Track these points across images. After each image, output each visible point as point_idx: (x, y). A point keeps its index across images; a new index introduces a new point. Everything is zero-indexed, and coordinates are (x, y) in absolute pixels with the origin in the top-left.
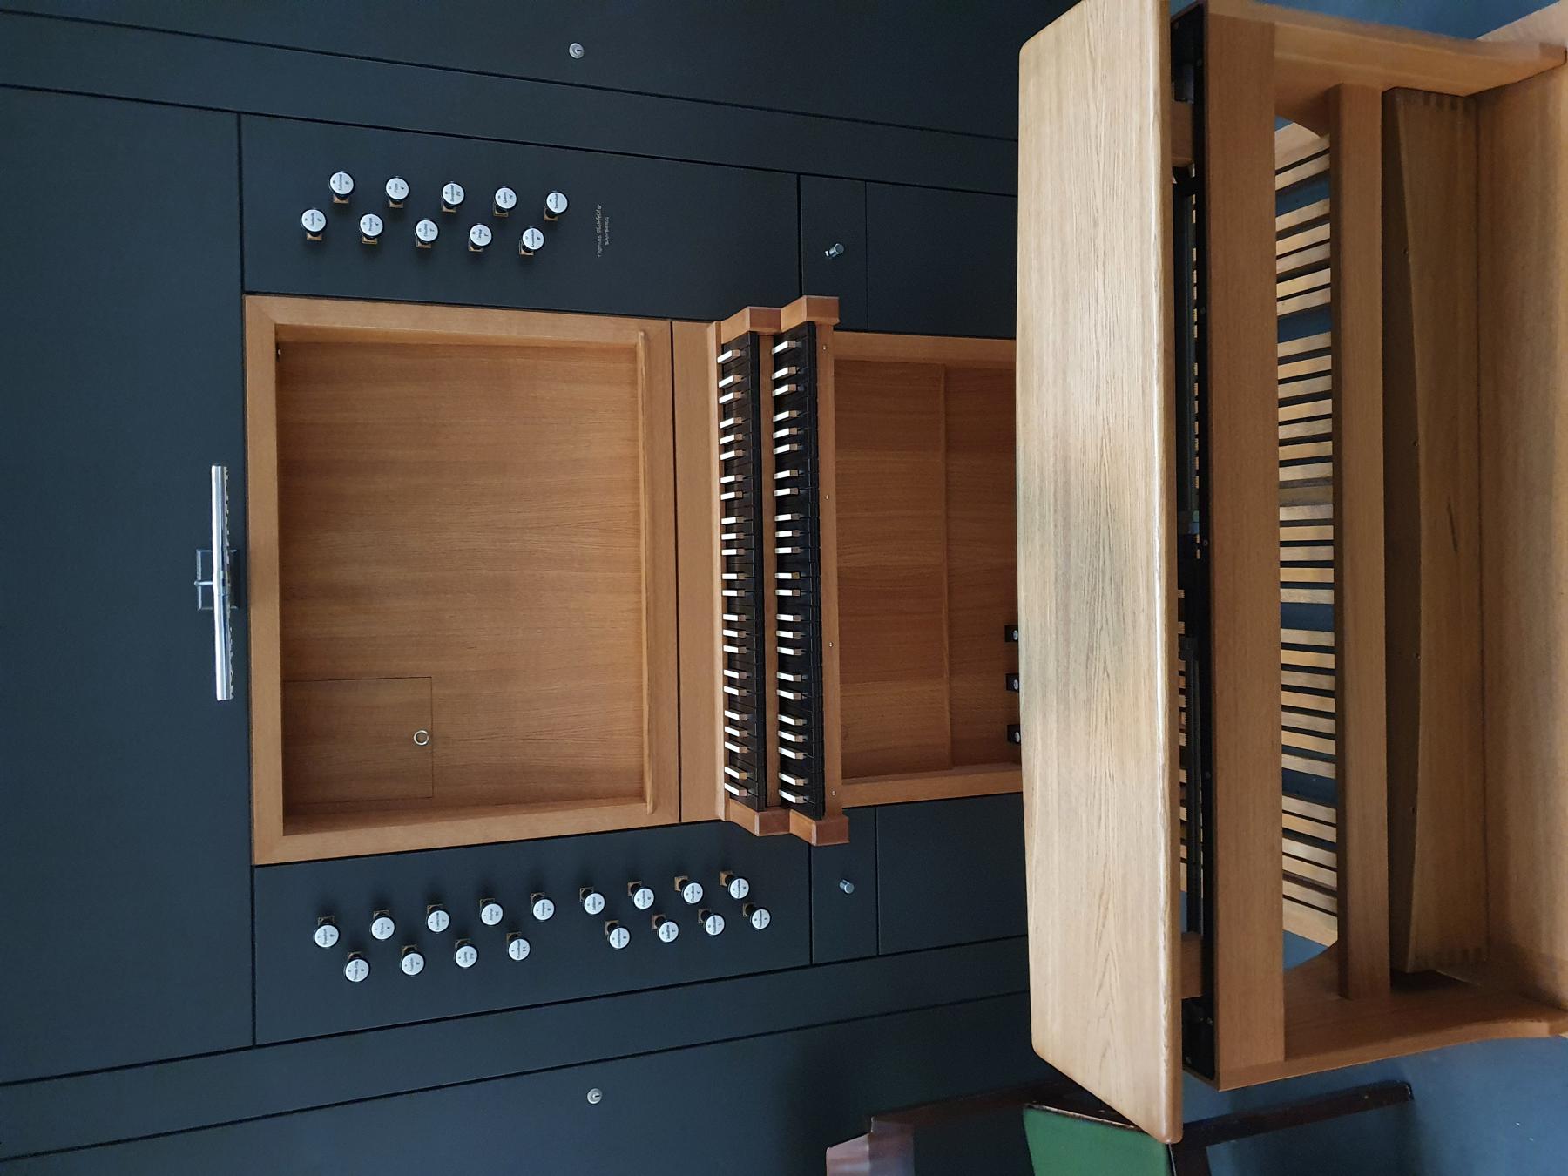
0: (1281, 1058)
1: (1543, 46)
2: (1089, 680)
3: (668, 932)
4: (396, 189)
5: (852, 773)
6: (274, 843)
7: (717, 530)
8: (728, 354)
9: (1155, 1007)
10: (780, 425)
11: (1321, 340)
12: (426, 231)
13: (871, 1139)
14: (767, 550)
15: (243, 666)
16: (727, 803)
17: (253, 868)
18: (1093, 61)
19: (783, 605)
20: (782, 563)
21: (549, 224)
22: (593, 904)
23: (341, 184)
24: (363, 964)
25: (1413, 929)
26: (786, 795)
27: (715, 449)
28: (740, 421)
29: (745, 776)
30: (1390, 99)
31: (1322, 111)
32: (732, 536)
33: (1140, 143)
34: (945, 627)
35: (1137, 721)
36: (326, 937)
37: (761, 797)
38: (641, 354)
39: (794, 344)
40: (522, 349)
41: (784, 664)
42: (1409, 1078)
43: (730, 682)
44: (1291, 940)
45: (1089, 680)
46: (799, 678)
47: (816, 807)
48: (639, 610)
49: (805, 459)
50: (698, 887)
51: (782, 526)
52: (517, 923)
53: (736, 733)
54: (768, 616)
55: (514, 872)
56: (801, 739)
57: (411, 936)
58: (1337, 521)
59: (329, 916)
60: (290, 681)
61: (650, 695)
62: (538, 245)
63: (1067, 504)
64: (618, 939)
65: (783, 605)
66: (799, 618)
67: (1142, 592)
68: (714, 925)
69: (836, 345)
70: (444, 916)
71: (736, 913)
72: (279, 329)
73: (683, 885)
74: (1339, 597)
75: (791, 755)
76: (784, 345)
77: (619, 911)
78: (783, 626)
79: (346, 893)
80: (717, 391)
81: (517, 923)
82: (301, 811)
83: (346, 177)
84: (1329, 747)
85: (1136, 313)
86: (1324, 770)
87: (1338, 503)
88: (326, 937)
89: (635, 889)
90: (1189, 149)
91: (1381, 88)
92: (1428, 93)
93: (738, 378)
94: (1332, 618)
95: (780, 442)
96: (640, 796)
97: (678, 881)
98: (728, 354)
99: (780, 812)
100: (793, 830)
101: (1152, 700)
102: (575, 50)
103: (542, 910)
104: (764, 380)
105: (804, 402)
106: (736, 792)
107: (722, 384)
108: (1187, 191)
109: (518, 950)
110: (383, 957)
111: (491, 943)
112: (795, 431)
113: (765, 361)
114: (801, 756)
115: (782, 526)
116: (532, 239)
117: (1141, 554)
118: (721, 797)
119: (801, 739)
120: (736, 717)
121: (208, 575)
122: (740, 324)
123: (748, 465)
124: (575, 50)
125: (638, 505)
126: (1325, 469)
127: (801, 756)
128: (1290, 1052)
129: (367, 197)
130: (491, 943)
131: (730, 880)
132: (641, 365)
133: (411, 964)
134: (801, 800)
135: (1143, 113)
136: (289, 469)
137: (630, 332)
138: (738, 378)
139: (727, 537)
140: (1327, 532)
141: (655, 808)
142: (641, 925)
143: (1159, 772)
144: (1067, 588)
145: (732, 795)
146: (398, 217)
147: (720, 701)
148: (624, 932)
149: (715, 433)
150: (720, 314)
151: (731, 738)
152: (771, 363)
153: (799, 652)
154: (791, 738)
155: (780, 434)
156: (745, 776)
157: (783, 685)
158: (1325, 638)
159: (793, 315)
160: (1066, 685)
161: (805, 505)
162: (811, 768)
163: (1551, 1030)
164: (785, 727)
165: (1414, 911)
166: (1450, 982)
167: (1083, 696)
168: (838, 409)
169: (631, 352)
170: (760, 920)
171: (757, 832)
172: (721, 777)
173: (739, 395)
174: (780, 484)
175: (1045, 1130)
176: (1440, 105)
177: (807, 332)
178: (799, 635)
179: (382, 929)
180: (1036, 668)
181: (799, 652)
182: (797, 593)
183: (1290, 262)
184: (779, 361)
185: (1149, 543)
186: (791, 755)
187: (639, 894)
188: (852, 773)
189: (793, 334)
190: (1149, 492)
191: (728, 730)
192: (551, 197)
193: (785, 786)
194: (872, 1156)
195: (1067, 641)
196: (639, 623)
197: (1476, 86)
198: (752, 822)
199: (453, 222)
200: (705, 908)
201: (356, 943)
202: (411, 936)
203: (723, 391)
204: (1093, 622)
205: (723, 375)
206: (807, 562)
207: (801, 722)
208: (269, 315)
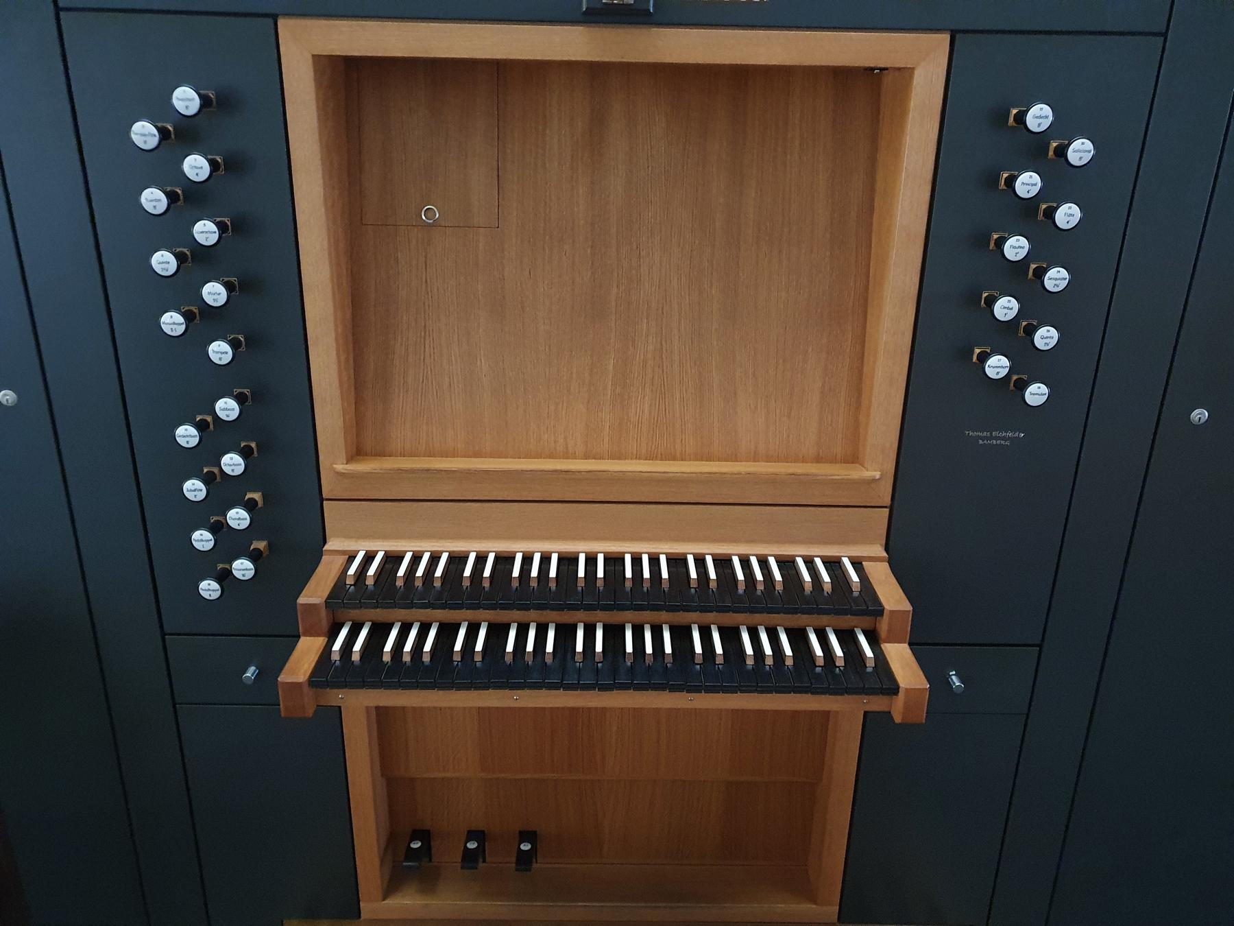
3: (194, 489)
4: (1068, 215)
17: (275, 18)
21: (1014, 385)
23: (1080, 151)
27: (744, 549)
34: (536, 776)
36: (185, 99)
39: (870, 664)
46: (478, 658)
49: (735, 673)
52: (205, 321)
66: (549, 660)
68: (202, 539)
72: (913, 69)
77: (217, 437)
79: (240, 124)
80: (811, 556)
81: (205, 321)
82: (348, 78)
88: (185, 99)
96: (357, 452)
100: (303, 639)
102: (1200, 415)
103: (220, 351)
104: (824, 619)
109: (172, 322)
114: (387, 658)
118: (349, 545)
119: (407, 658)
122: (892, 596)
124: (1200, 415)
127: (387, 658)
133: (153, 199)
137: (877, 467)
139: (645, 558)
142: (202, 460)
145: (351, 558)
146: (1034, 217)
149: (762, 550)
153: (508, 659)
155: (764, 637)
162: (371, 670)
168: (795, 714)
171: (302, 600)
172: (372, 546)
177: (884, 681)
178: (529, 660)
182: (579, 658)
198: (315, 593)
199: (1022, 277)
206: (615, 670)
207: (426, 659)
208: (925, 62)
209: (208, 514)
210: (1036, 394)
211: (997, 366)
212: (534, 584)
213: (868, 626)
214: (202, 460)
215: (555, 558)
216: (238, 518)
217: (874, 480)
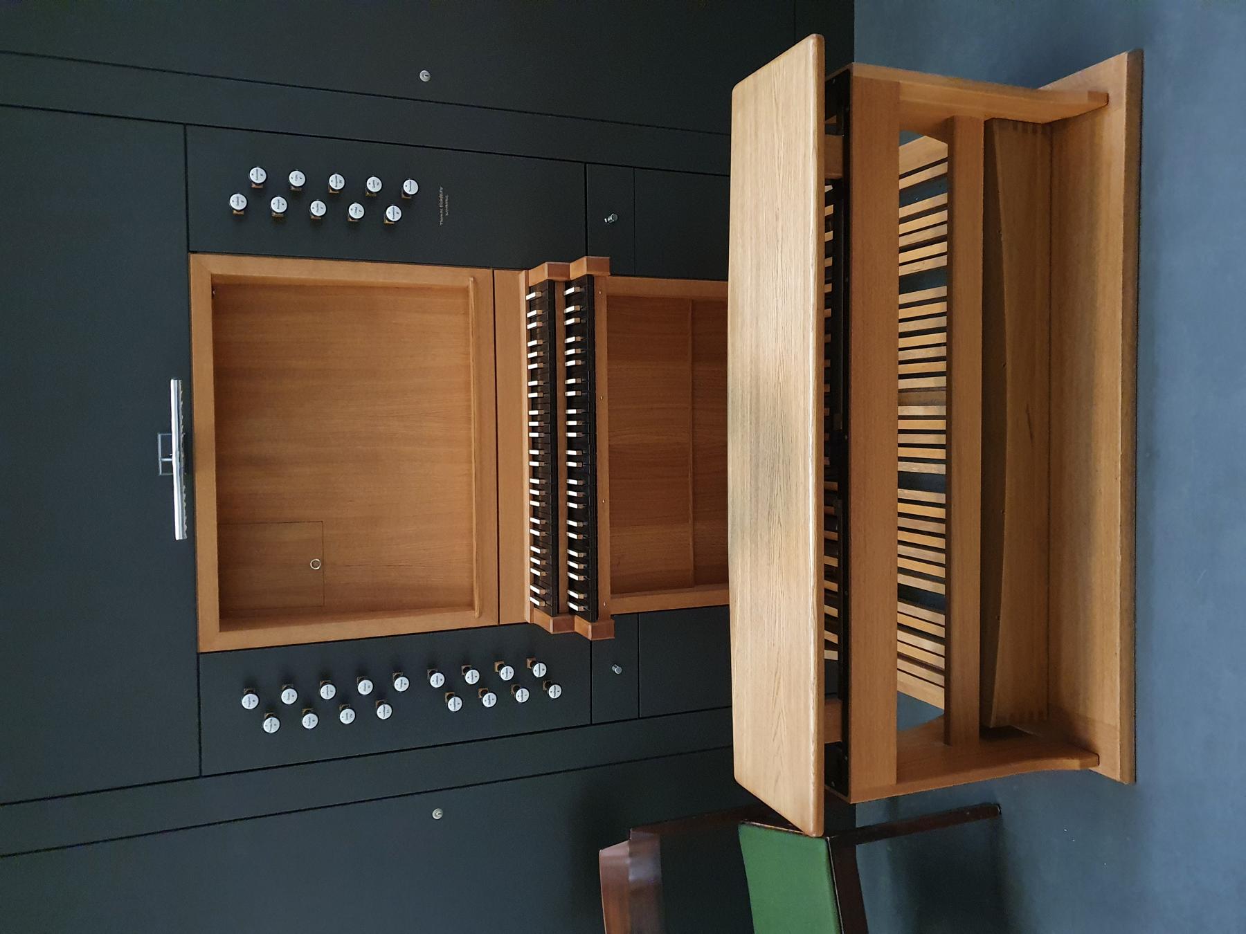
0: (894, 781)
1: (1090, 93)
2: (769, 528)
5: (617, 590)
6: (213, 637)
7: (526, 419)
8: (533, 295)
9: (807, 747)
10: (569, 346)
11: (942, 291)
12: (318, 209)
13: (630, 844)
14: (560, 433)
15: (191, 514)
16: (532, 611)
17: (198, 654)
18: (777, 105)
19: (571, 473)
20: (571, 444)
21: (405, 202)
22: (437, 680)
23: (257, 176)
24: (275, 721)
25: (995, 700)
26: (572, 606)
28: (541, 342)
29: (544, 592)
30: (988, 124)
31: (945, 129)
32: (536, 424)
33: (804, 165)
35: (797, 556)
36: (249, 702)
37: (555, 606)
38: (471, 294)
39: (578, 289)
40: (386, 289)
41: (572, 514)
42: (1000, 800)
43: (534, 526)
44: (906, 703)
45: (769, 528)
46: (581, 525)
47: (592, 614)
48: (470, 475)
49: (586, 371)
50: (510, 669)
51: (570, 417)
52: (383, 693)
53: (538, 562)
54: (561, 480)
55: (381, 658)
56: (582, 566)
57: (309, 702)
58: (948, 417)
59: (251, 687)
60: (224, 524)
61: (477, 535)
62: (397, 217)
63: (758, 409)
64: (454, 704)
65: (571, 473)
67: (801, 470)
68: (522, 696)
69: (610, 285)
70: (332, 688)
71: (537, 687)
72: (213, 277)
73: (500, 667)
74: (948, 469)
75: (575, 577)
76: (571, 290)
77: (454, 686)
78: (571, 487)
81: (383, 693)
82: (230, 616)
83: (261, 171)
84: (939, 572)
85: (800, 281)
86: (940, 589)
87: (949, 404)
88: (249, 702)
89: (466, 670)
90: (839, 167)
91: (983, 119)
92: (1015, 122)
93: (540, 312)
94: (940, 484)
95: (570, 358)
96: (471, 606)
97: (497, 665)
98: (533, 295)
99: (570, 617)
100: (576, 630)
101: (807, 544)
102: (424, 76)
103: (401, 684)
105: (586, 330)
106: (537, 603)
107: (530, 315)
108: (838, 196)
109: (383, 712)
110: (289, 716)
111: (364, 708)
112: (579, 351)
113: (559, 301)
115: (570, 417)
116: (393, 214)
117: (801, 445)
119: (582, 566)
120: (538, 551)
121: (168, 452)
122: (541, 274)
123: (547, 374)
124: (424, 76)
125: (469, 400)
126: (942, 381)
127: (582, 578)
128: (900, 779)
129: (275, 184)
130: (364, 708)
131: (533, 664)
132: (472, 302)
133: (309, 721)
134: (582, 608)
135: (806, 146)
136: (222, 374)
137: (463, 277)
138: (540, 312)
140: (940, 425)
141: (481, 614)
142: (471, 695)
143: (810, 591)
144: (757, 466)
145: (535, 606)
147: (527, 540)
148: (458, 700)
150: (528, 266)
151: (535, 566)
152: (563, 302)
153: (581, 506)
154: (575, 565)
156: (544, 592)
157: (570, 529)
158: (941, 498)
159: (578, 269)
160: (756, 531)
161: (586, 403)
162: (589, 586)
163: (1081, 766)
164: (571, 558)
165: (997, 686)
166: (1021, 734)
167: (766, 539)
169: (465, 291)
170: (554, 692)
171: (551, 631)
172: (528, 593)
173: (540, 324)
174: (569, 387)
175: (752, 837)
176: (1025, 131)
177: (588, 282)
178: (581, 494)
179: (288, 697)
180: (738, 519)
181: (581, 506)
182: (580, 465)
183: (916, 236)
184: (569, 300)
185: (806, 437)
186: (575, 577)
187: (469, 674)
188: (617, 590)
189: (578, 282)
190: (806, 404)
191: (534, 560)
192: (407, 183)
193: (572, 599)
194: (631, 855)
195: (757, 501)
196: (470, 485)
197: (1048, 117)
200: (516, 683)
201: (271, 706)
202: (309, 702)
203: (530, 320)
204: (772, 490)
205: (530, 309)
206: (587, 443)
207: (582, 555)
208: (207, 268)
209: (505, 691)
210: (410, 187)
211: (393, 214)
212: (581, 494)
213: (563, 286)
214: (471, 695)
215: (533, 481)
216: (506, 674)
217: (475, 281)
